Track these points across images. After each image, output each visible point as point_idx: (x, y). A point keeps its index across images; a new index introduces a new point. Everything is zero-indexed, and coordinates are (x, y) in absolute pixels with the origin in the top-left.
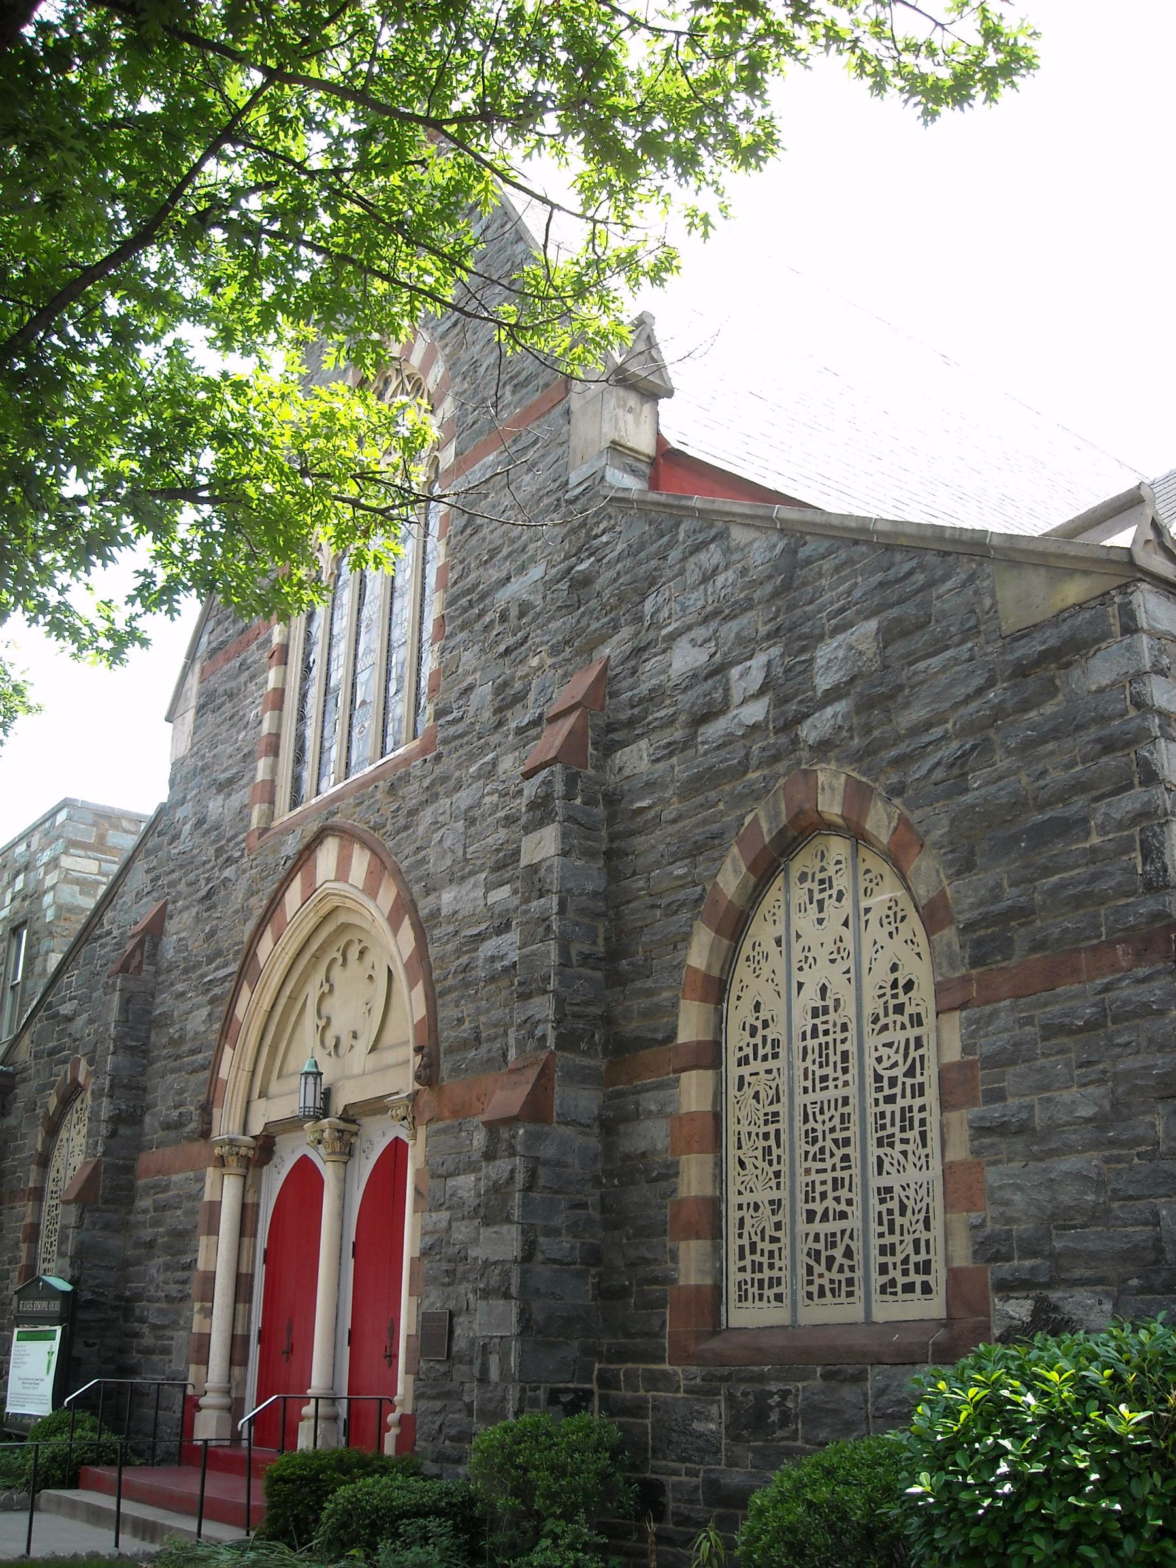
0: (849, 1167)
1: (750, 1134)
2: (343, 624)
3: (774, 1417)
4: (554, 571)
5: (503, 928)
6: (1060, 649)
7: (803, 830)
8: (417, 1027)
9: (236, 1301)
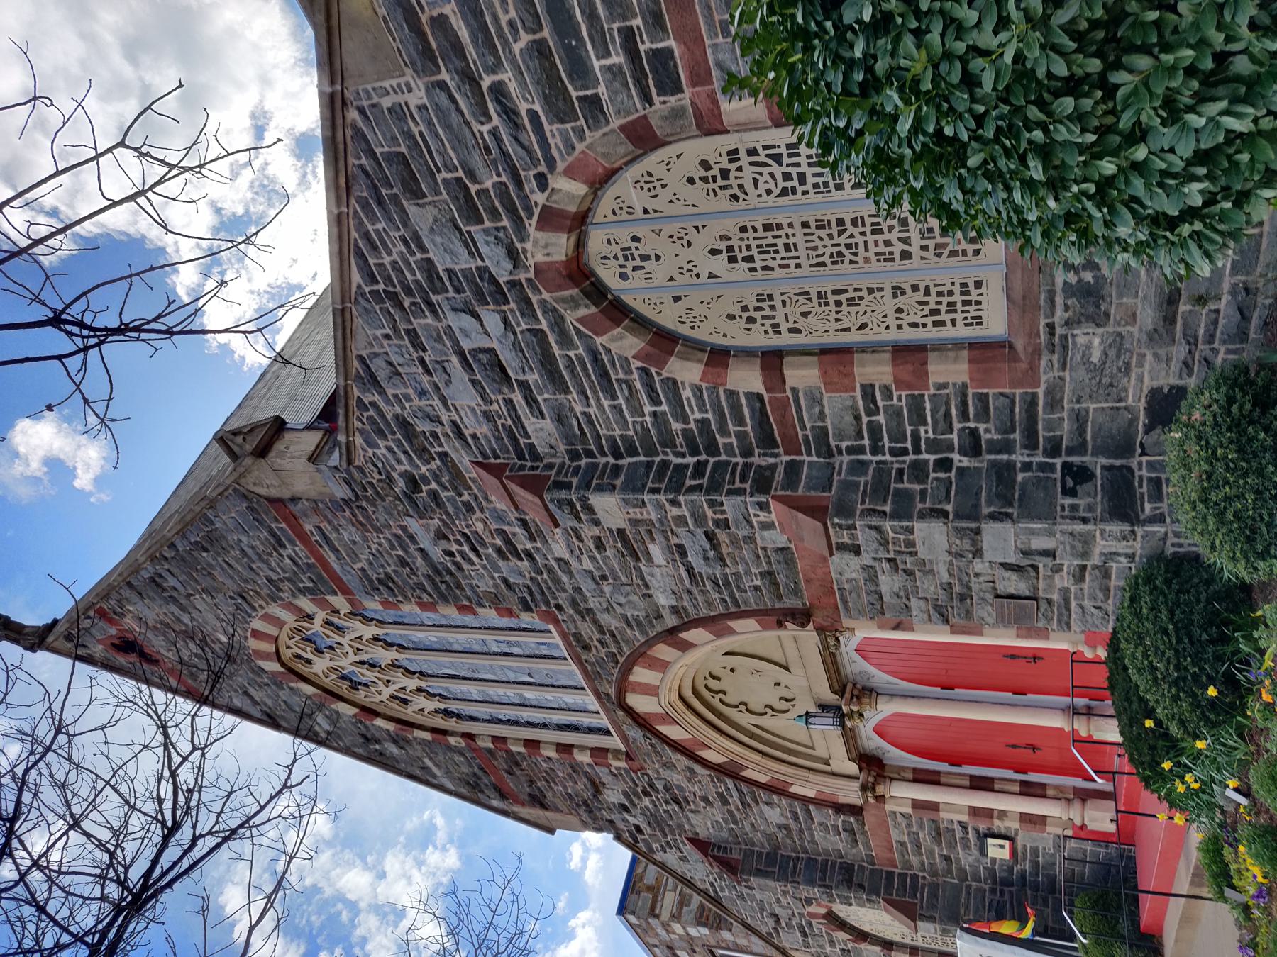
0: (862, 217)
1: (837, 320)
2: (473, 690)
3: (1088, 276)
4: (411, 512)
5: (682, 550)
6: (404, 9)
7: (578, 273)
8: (765, 627)
9: (992, 790)
